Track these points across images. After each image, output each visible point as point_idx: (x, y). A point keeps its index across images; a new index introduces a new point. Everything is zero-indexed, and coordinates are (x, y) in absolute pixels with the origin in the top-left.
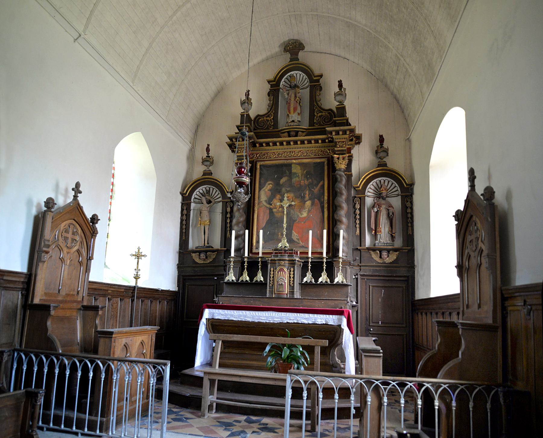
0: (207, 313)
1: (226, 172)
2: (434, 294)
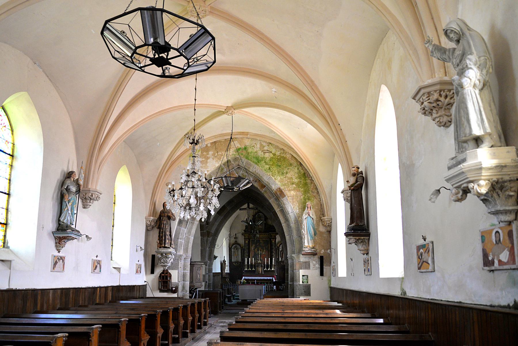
0: (243, 278)
1: (241, 240)
2: (122, 168)
